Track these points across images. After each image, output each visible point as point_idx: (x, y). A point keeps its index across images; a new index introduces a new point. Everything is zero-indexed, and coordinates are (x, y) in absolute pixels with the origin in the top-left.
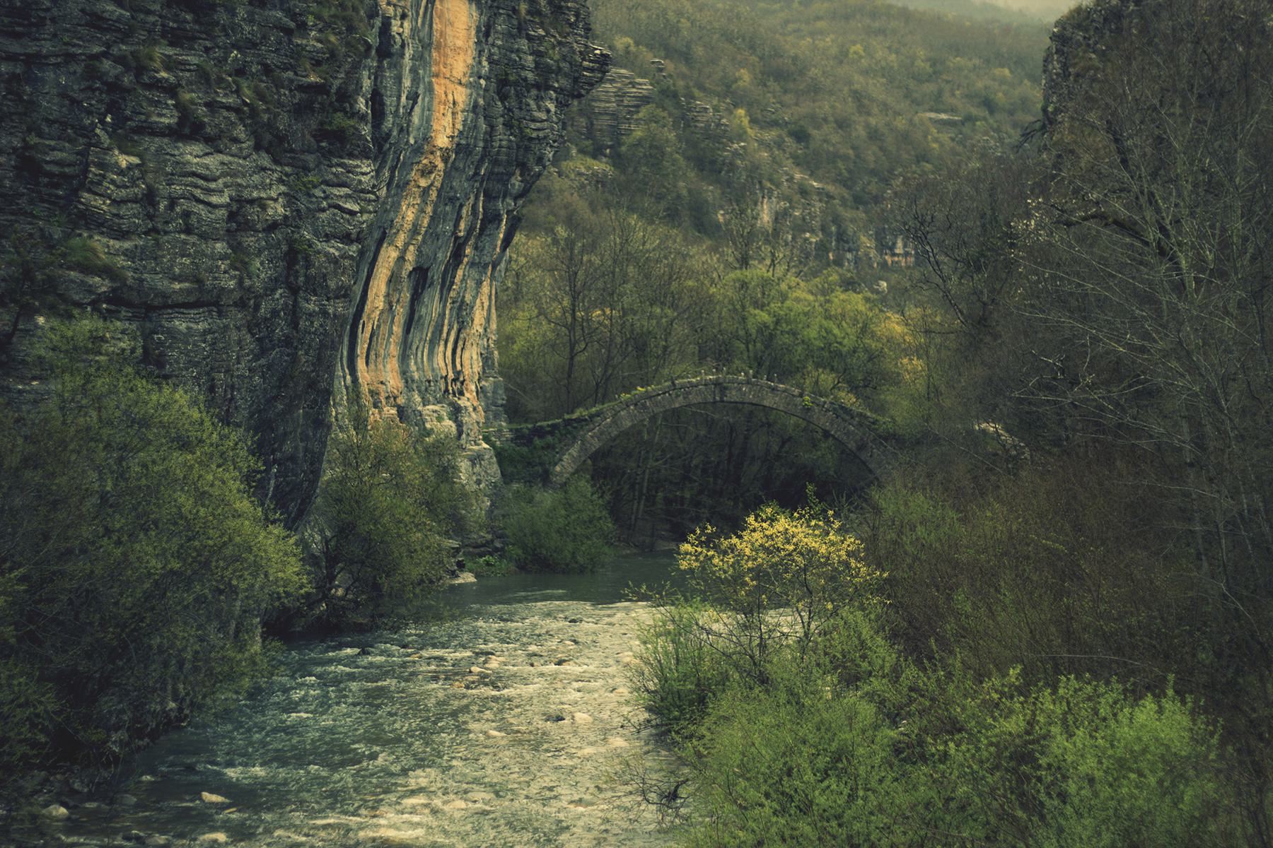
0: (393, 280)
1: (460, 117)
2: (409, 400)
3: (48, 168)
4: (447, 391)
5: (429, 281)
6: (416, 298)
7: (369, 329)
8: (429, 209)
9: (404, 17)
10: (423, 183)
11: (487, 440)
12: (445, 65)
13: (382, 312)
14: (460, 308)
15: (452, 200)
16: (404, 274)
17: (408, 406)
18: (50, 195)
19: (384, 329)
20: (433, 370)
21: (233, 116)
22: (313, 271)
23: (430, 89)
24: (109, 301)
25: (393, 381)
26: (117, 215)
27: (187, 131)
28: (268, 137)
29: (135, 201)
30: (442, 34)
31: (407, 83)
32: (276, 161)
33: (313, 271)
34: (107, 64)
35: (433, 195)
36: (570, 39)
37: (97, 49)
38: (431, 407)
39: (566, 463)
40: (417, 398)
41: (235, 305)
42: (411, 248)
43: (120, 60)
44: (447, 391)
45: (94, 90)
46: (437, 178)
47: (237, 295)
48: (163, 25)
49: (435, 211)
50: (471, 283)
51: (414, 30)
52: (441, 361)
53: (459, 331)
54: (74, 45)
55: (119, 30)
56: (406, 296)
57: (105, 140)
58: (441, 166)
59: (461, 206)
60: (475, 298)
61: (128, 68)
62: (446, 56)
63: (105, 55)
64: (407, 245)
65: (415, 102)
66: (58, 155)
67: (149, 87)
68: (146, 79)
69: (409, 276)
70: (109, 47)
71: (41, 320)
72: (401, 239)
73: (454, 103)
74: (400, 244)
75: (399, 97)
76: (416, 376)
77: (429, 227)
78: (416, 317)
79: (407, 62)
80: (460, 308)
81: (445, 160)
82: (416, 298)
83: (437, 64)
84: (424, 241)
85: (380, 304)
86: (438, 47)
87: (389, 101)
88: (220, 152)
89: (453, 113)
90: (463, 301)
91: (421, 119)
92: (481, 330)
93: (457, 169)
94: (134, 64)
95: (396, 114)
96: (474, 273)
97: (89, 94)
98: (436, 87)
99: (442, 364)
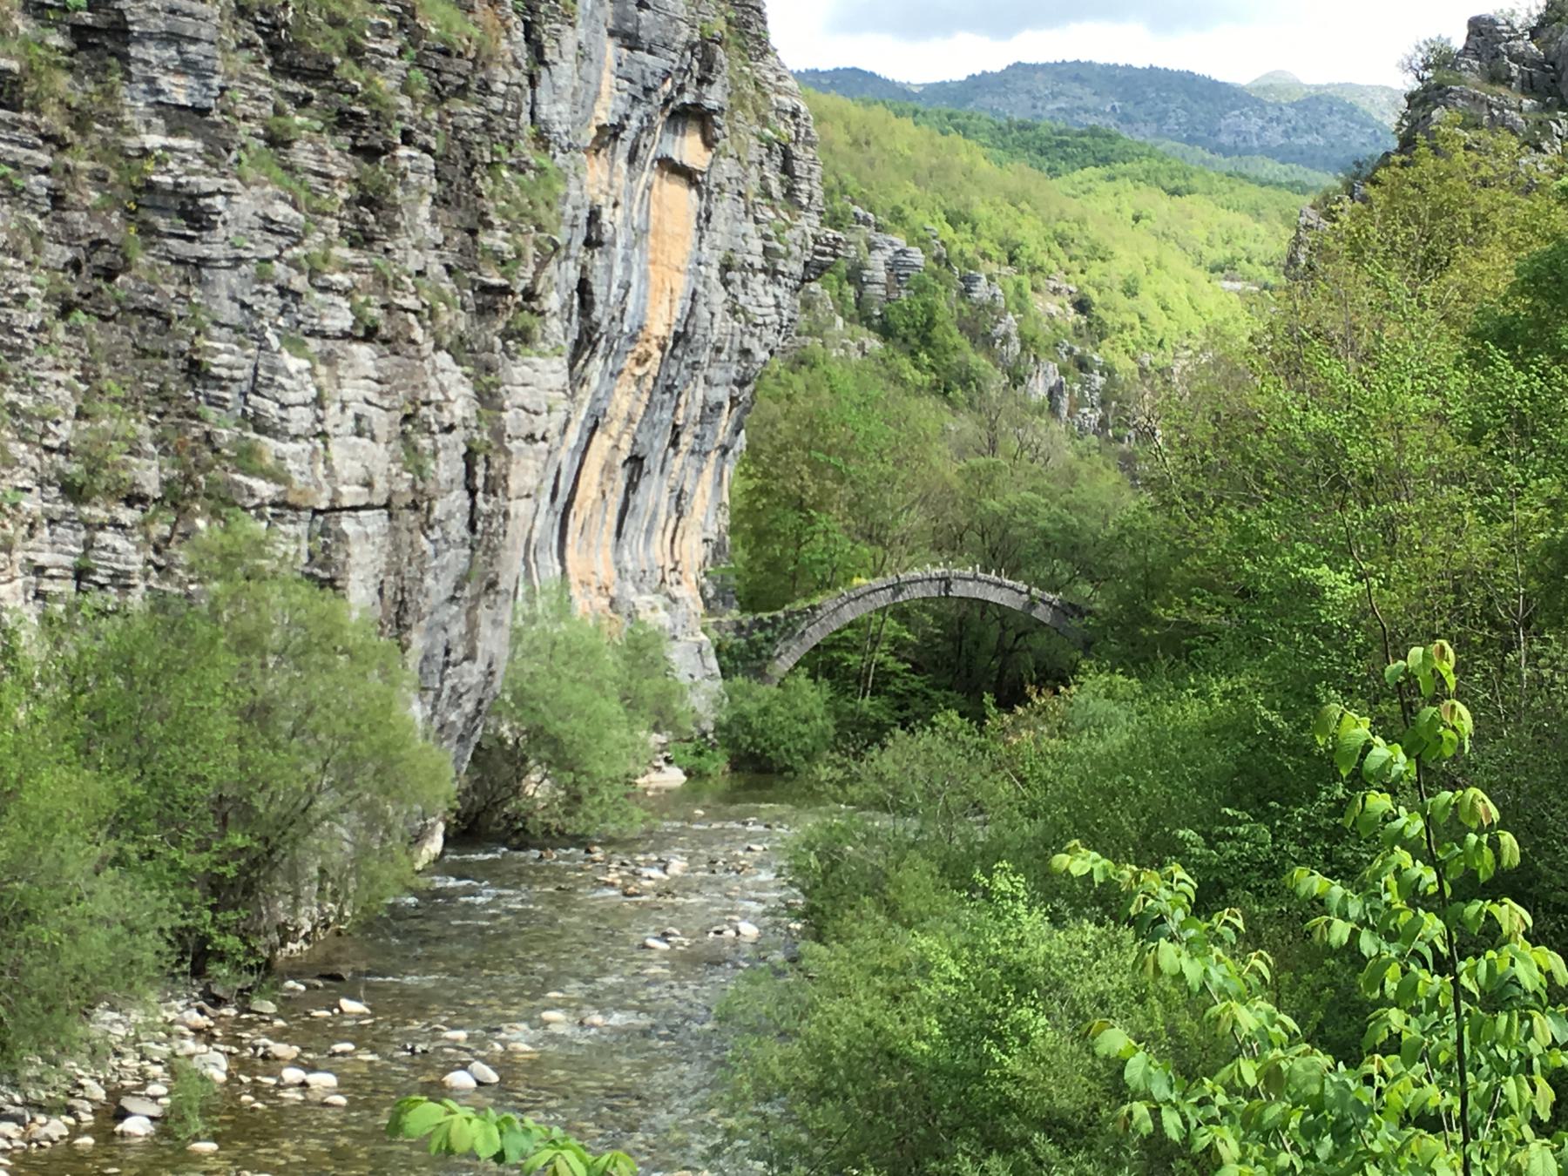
0: (608, 468)
1: (678, 305)
2: (621, 590)
3: (214, 370)
4: (663, 580)
5: (645, 470)
6: (632, 487)
7: (580, 518)
8: (645, 397)
9: (616, 205)
10: (639, 371)
11: (704, 631)
12: (663, 252)
13: (594, 501)
14: (679, 498)
15: (669, 388)
16: (619, 463)
17: (620, 596)
18: (218, 398)
19: (597, 518)
20: (649, 559)
21: (411, 317)
22: (492, 472)
23: (645, 277)
24: (274, 505)
25: (603, 568)
26: (282, 419)
27: (361, 333)
28: (447, 340)
29: (305, 405)
30: (660, 220)
31: (618, 271)
32: (458, 362)
33: (492, 472)
34: (278, 268)
35: (649, 382)
36: (799, 222)
37: (271, 252)
38: (645, 598)
39: (784, 660)
40: (630, 588)
41: (407, 507)
42: (626, 437)
43: (293, 263)
44: (663, 580)
45: (264, 294)
46: (653, 366)
47: (409, 498)
48: (342, 227)
49: (650, 400)
50: (691, 472)
51: (628, 220)
52: (658, 550)
53: (678, 519)
54: (247, 249)
55: (291, 233)
56: (621, 482)
57: (275, 343)
58: (657, 354)
59: (679, 394)
60: (695, 487)
61: (300, 270)
62: (663, 242)
63: (278, 258)
64: (621, 434)
65: (627, 292)
66: (225, 358)
67: (325, 289)
68: (320, 283)
69: (624, 464)
70: (281, 250)
71: (201, 523)
72: (615, 428)
73: (672, 291)
74: (614, 433)
75: (609, 287)
76: (630, 566)
77: (645, 414)
78: (631, 507)
79: (619, 251)
80: (679, 498)
81: (662, 348)
82: (632, 487)
83: (654, 250)
84: (639, 430)
85: (594, 493)
86: (656, 234)
87: (598, 290)
88: (397, 354)
89: (671, 301)
90: (682, 490)
91: (636, 307)
92: (702, 519)
93: (675, 358)
94: (306, 266)
95: (606, 303)
96: (694, 460)
97: (260, 297)
98: (652, 274)
99: (659, 553)
